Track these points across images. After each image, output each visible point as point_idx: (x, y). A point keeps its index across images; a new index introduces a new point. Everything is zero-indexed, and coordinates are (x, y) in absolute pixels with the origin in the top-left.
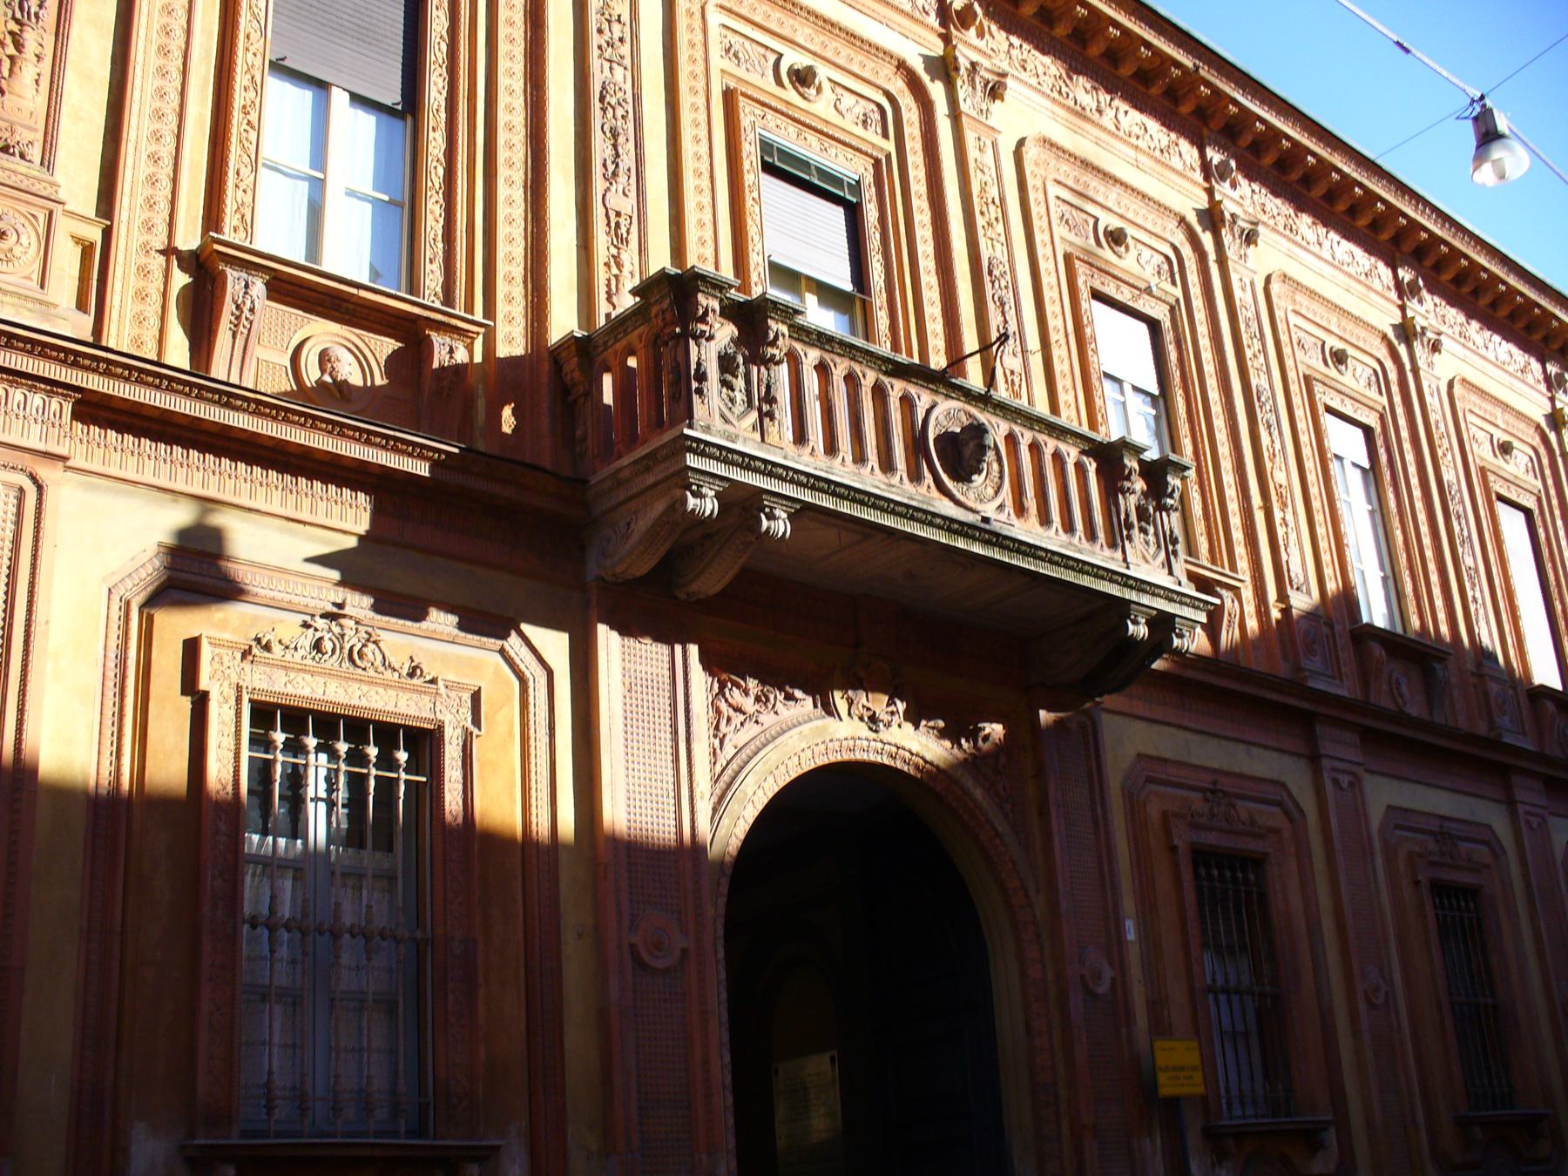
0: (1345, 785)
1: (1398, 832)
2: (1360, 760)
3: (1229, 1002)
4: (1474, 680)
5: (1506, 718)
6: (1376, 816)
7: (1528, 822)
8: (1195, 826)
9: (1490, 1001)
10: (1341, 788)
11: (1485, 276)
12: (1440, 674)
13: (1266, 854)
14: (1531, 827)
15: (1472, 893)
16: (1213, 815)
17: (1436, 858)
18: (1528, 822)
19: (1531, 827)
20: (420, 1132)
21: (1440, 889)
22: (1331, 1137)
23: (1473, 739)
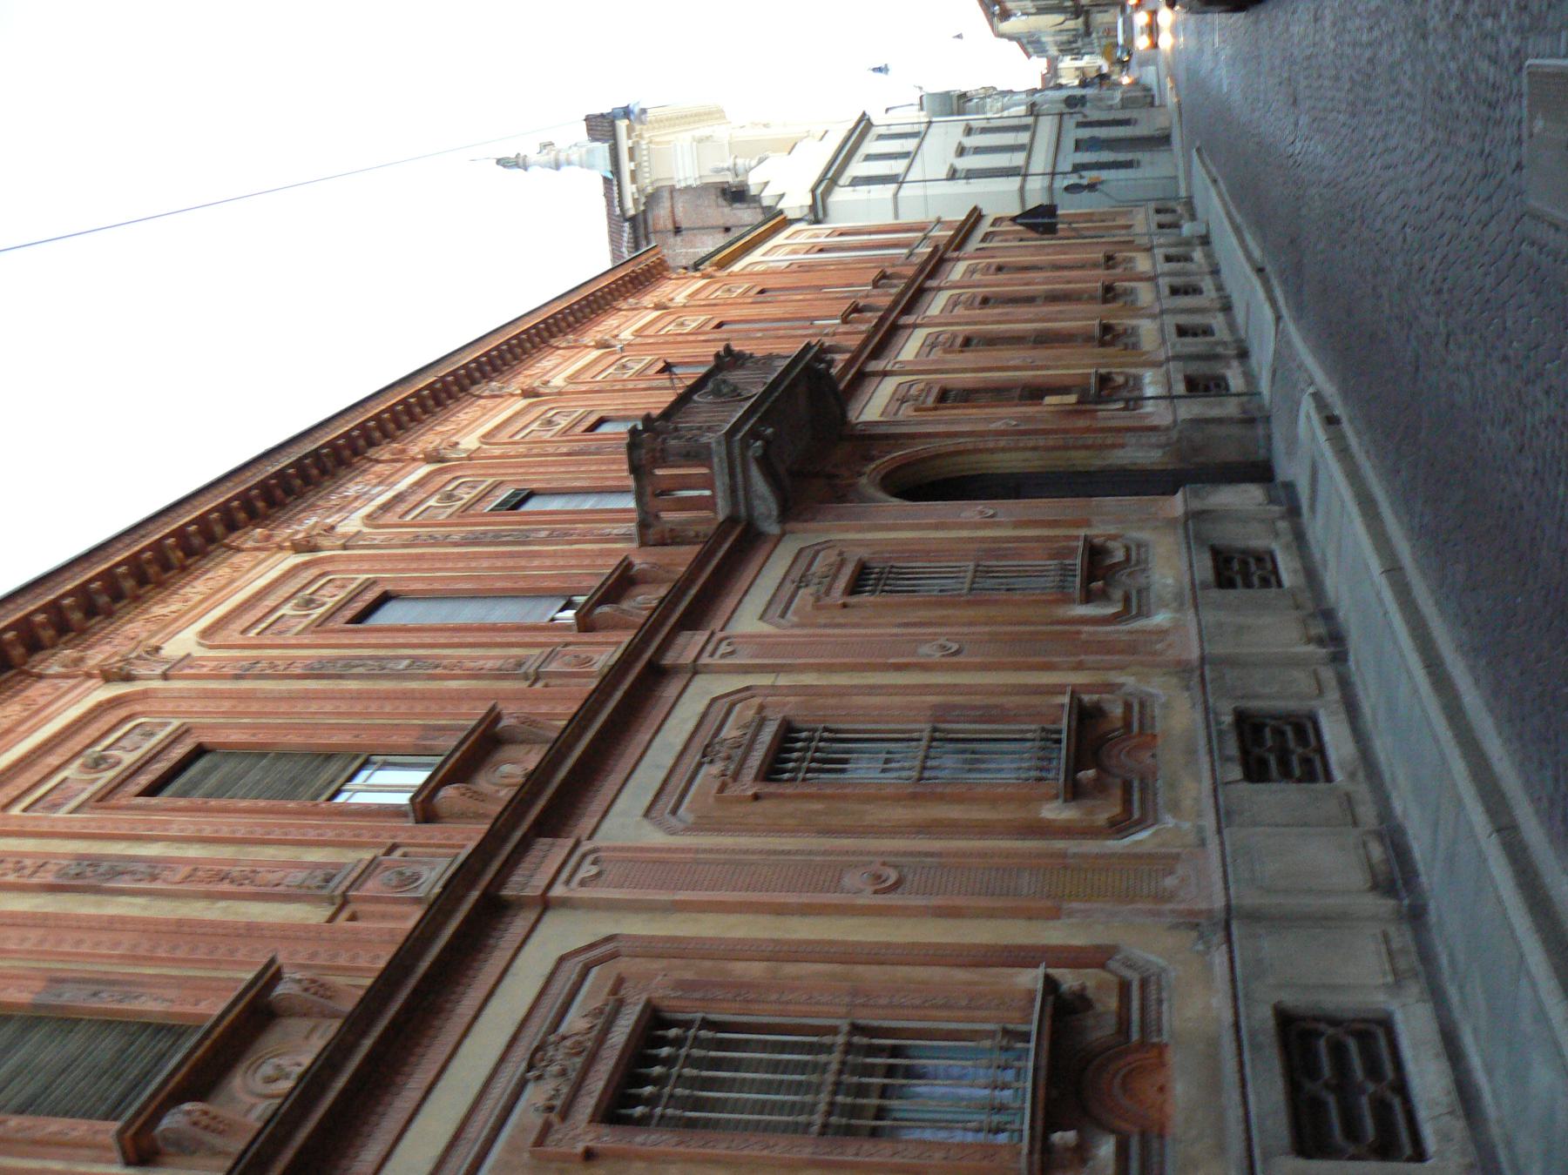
0: (729, 649)
1: (682, 811)
2: (707, 634)
3: (932, 768)
4: (539, 686)
5: (596, 657)
6: (654, 837)
7: (723, 656)
8: (736, 776)
9: (840, 1039)
10: (599, 874)
11: (193, 528)
12: (513, 721)
13: (648, 1003)
14: (732, 653)
15: (788, 733)
16: (729, 758)
17: (823, 590)
18: (723, 656)
19: (732, 653)
20: (1059, 741)
21: (772, 771)
22: (1069, 979)
23: (908, 287)
